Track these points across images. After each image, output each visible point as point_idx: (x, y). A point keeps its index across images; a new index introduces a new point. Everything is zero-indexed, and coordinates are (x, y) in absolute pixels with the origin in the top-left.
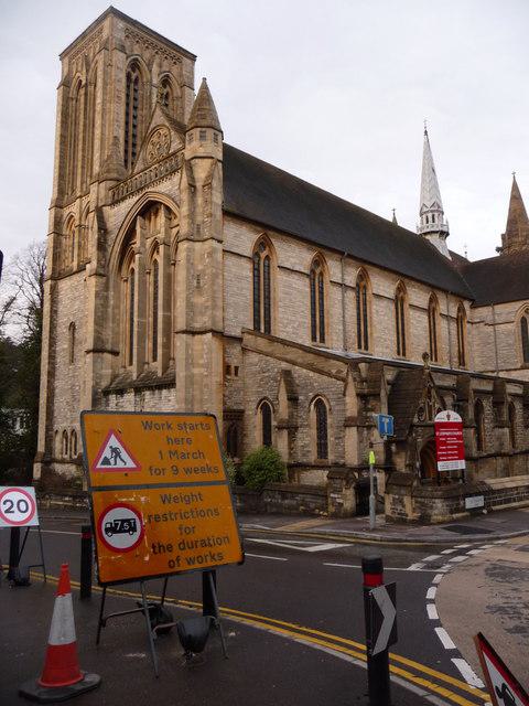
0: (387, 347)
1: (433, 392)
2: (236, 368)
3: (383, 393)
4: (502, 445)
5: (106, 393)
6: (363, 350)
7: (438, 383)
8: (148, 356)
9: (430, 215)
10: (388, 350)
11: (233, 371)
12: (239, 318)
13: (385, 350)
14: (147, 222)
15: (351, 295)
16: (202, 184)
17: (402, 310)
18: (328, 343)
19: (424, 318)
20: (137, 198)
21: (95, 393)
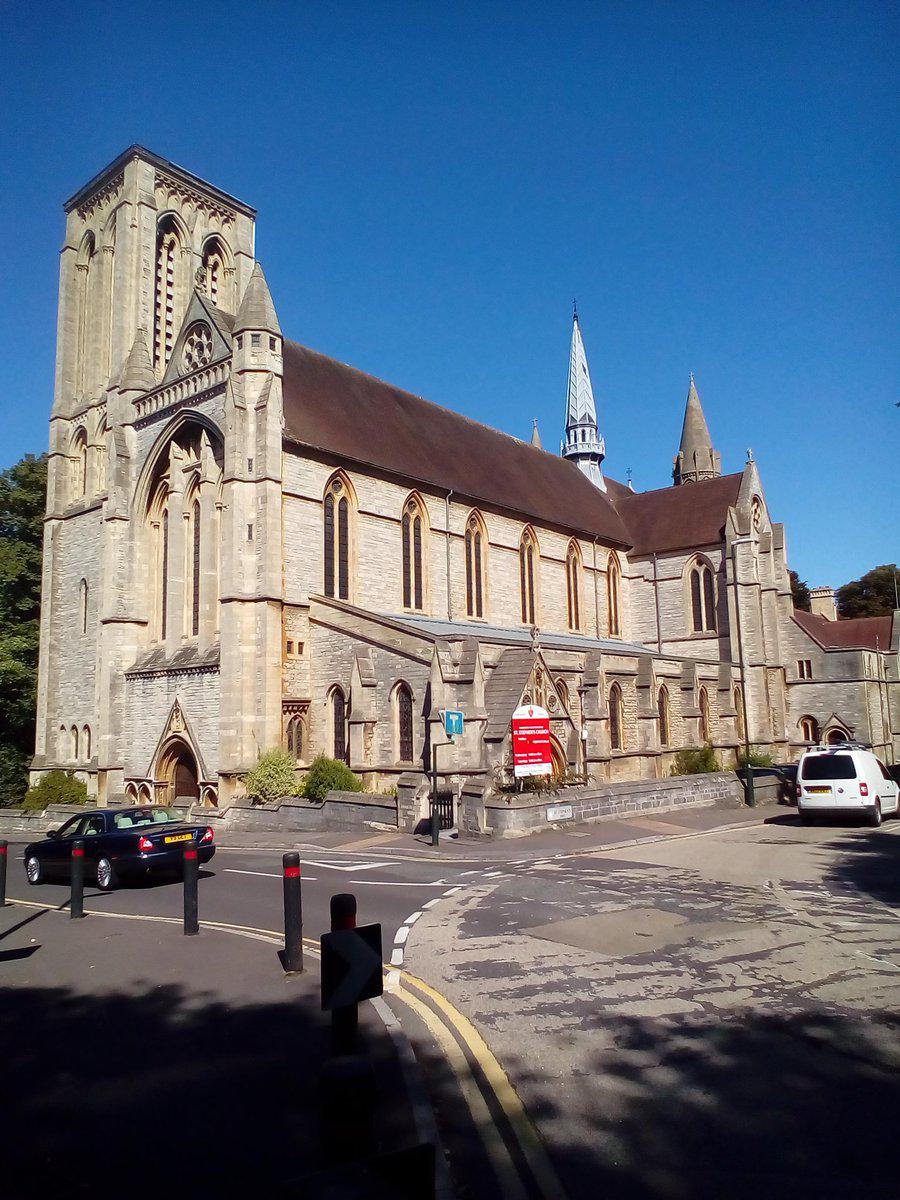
0: (508, 613)
1: (545, 676)
2: (301, 644)
3: (477, 679)
4: (647, 739)
5: (131, 676)
6: (574, 630)
7: (551, 663)
8: (188, 628)
9: (579, 430)
10: (510, 617)
11: (296, 647)
12: (305, 580)
13: (505, 617)
14: (185, 452)
15: (460, 545)
16: (254, 406)
17: (530, 563)
18: (426, 609)
19: (561, 572)
21: (115, 677)
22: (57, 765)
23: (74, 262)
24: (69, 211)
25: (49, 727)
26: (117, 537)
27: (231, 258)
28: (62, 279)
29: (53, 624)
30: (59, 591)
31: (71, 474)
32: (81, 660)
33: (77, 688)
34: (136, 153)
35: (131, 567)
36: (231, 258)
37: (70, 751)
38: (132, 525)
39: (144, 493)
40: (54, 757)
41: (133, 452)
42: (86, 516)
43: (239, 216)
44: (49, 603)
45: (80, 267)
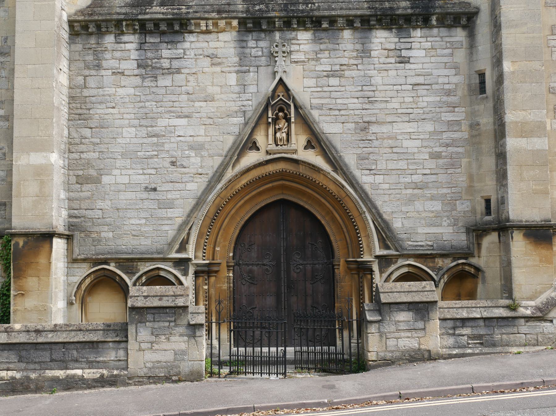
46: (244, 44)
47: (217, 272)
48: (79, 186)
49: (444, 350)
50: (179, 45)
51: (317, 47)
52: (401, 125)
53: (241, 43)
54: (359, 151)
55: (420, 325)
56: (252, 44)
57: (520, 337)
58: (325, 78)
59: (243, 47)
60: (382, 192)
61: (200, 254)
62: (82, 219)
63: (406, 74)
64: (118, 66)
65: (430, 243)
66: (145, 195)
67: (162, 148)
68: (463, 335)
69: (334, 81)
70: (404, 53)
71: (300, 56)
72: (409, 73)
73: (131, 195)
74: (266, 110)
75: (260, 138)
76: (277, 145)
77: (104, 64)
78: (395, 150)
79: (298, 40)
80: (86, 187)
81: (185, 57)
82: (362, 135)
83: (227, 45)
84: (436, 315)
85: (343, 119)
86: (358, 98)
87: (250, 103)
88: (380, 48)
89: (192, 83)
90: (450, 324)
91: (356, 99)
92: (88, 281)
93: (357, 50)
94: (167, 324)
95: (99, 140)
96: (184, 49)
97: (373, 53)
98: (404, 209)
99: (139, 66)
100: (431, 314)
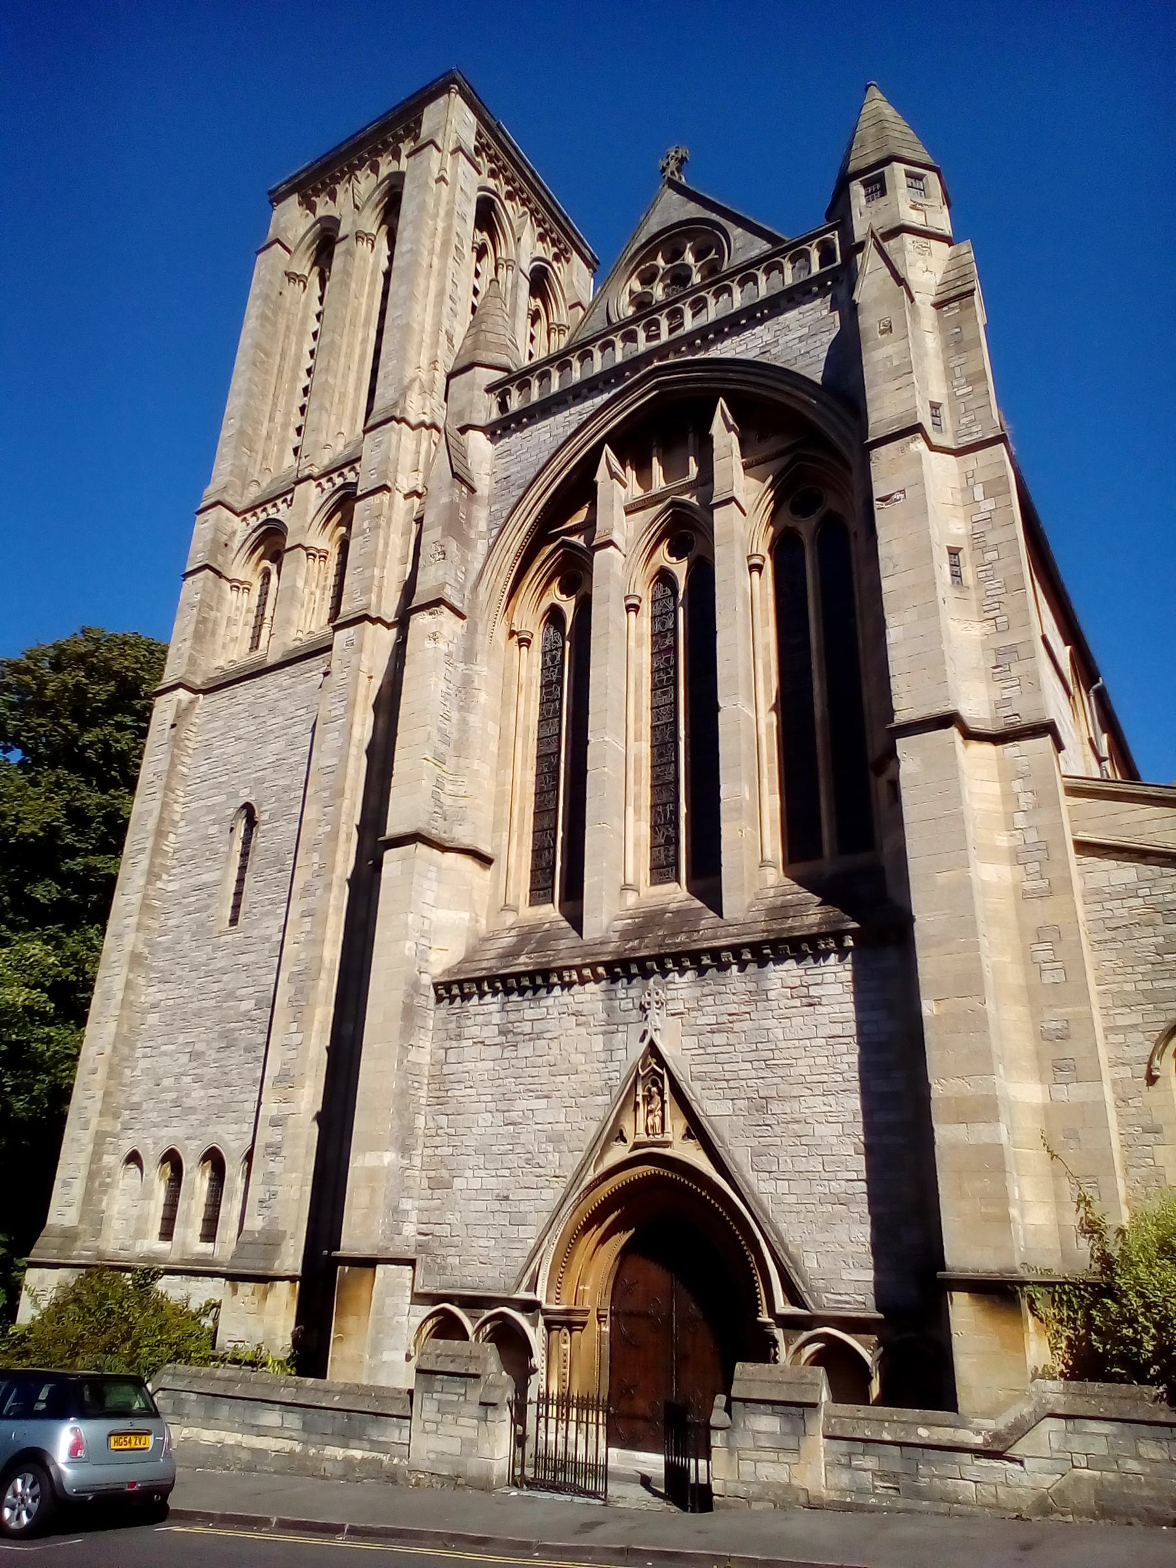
16: (932, 299)
20: (606, 396)
22: (100, 1255)
23: (282, 268)
24: (277, 198)
25: (96, 1156)
26: (442, 646)
27: (563, 311)
28: (255, 289)
29: (146, 907)
30: (172, 837)
31: (227, 610)
32: (216, 987)
33: (195, 1056)
34: (455, 81)
35: (464, 721)
36: (563, 311)
37: (143, 1219)
38: (471, 632)
39: (507, 561)
40: (97, 1234)
41: (484, 484)
42: (268, 679)
43: (575, 257)
44: (144, 861)
45: (291, 277)
46: (613, 995)
47: (584, 1324)
48: (430, 1192)
49: (832, 1493)
50: (542, 1003)
51: (697, 992)
52: (811, 1101)
53: (610, 995)
54: (754, 1142)
55: (791, 1443)
56: (621, 994)
57: (966, 1486)
58: (709, 1035)
59: (611, 999)
60: (787, 1208)
61: (553, 1296)
62: (430, 1237)
63: (815, 1023)
64: (478, 1033)
65: (860, 1298)
66: (496, 1206)
67: (518, 1141)
68: (865, 1470)
69: (719, 1039)
70: (813, 991)
71: (680, 1006)
72: (822, 1019)
73: (481, 1206)
74: (635, 1084)
75: (628, 1127)
76: (648, 1135)
77: (467, 1032)
78: (804, 1140)
79: (674, 983)
80: (438, 1193)
81: (548, 1017)
82: (758, 1118)
83: (595, 997)
84: (817, 1425)
85: (731, 1094)
86: (751, 1062)
87: (617, 1074)
88: (779, 985)
89: (555, 1050)
90: (843, 1446)
91: (749, 1064)
92: (430, 1324)
93: (750, 992)
94: (455, 1398)
95: (453, 1130)
96: (547, 1007)
97: (771, 995)
98: (820, 1237)
99: (502, 1033)
100: (808, 1425)
